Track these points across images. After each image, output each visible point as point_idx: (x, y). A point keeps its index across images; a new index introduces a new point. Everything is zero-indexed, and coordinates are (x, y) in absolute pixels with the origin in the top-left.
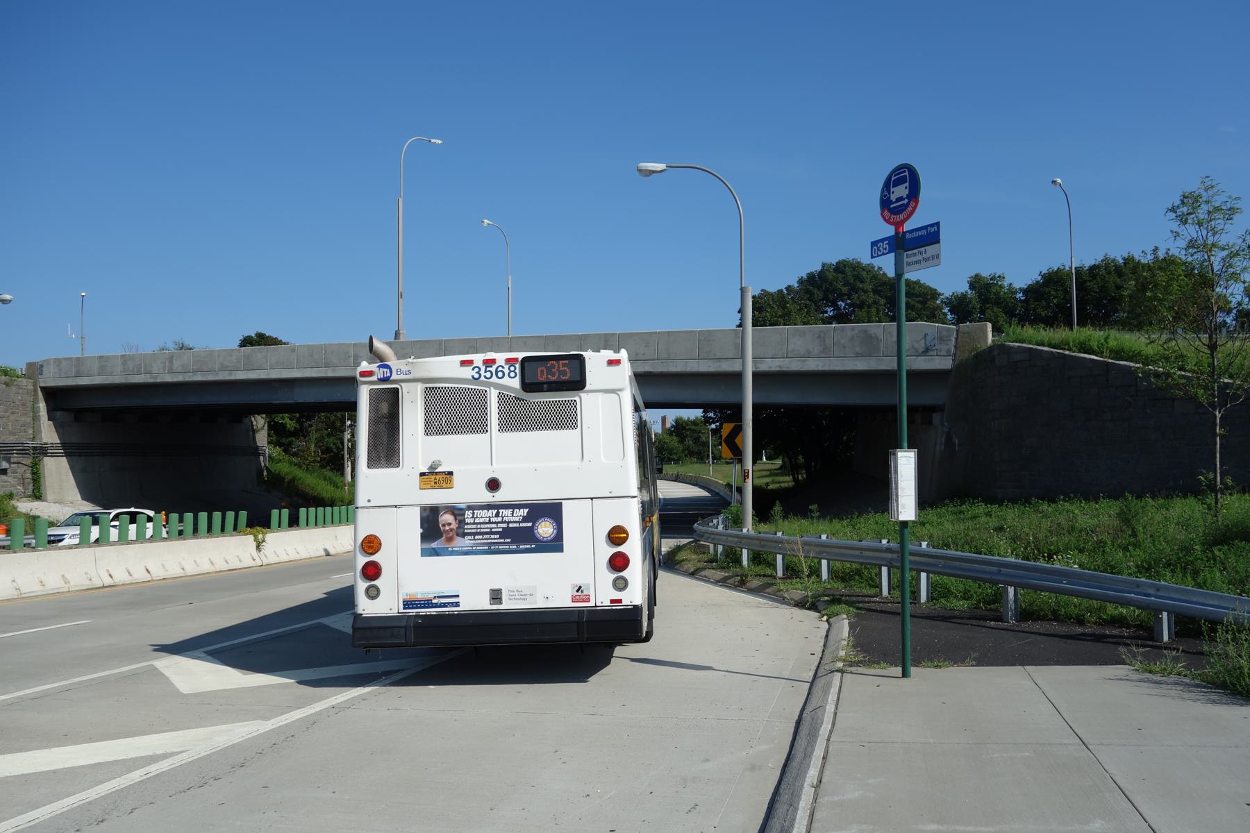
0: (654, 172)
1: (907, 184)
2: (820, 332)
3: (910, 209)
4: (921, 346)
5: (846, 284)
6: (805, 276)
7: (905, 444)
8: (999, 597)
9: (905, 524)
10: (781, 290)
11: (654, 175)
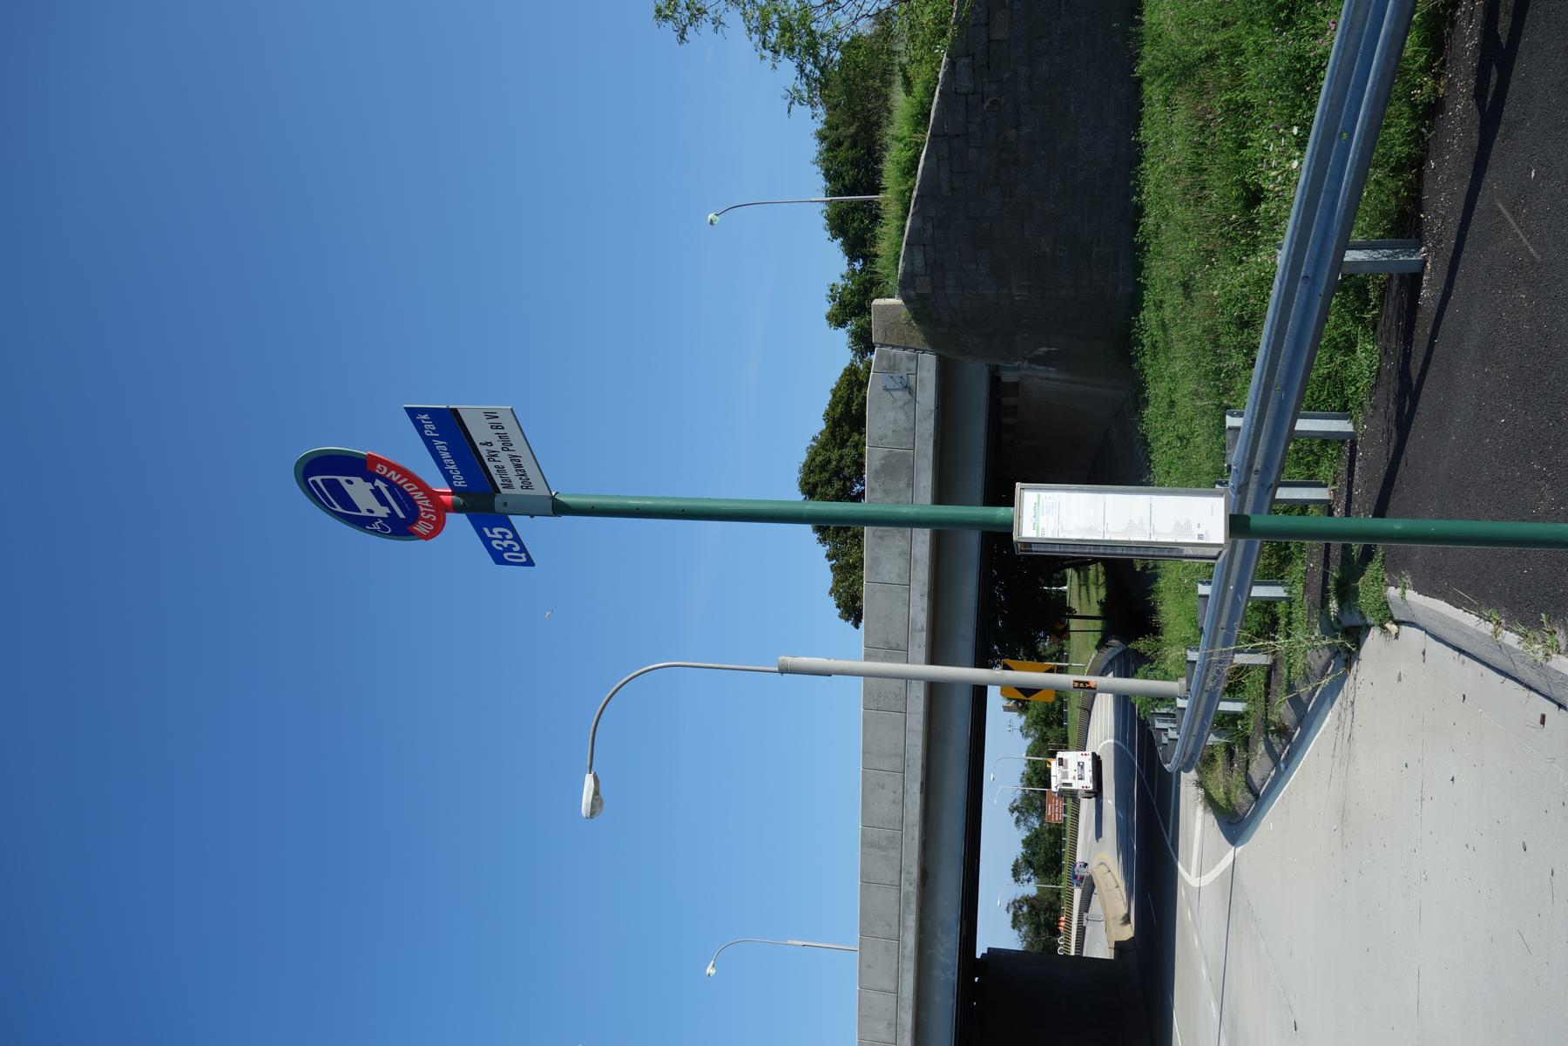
0: (596, 793)
1: (342, 479)
2: (874, 536)
3: (394, 477)
4: (902, 396)
5: (829, 482)
6: (817, 536)
7: (1000, 512)
8: (1354, 286)
9: (1237, 525)
10: (832, 566)
11: (602, 793)
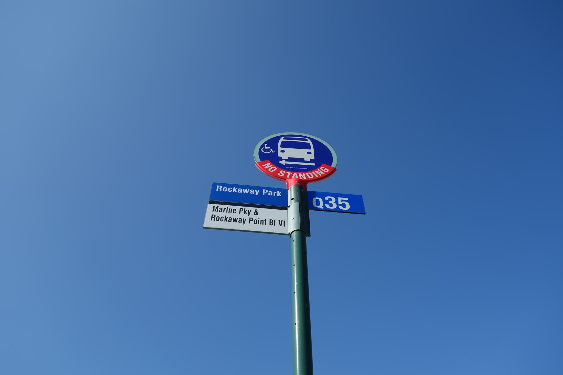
1: (312, 150)
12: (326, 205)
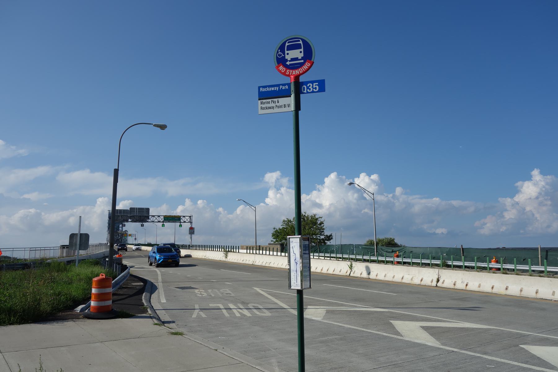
1: (302, 50)
3: (305, 67)
12: (286, 63)
